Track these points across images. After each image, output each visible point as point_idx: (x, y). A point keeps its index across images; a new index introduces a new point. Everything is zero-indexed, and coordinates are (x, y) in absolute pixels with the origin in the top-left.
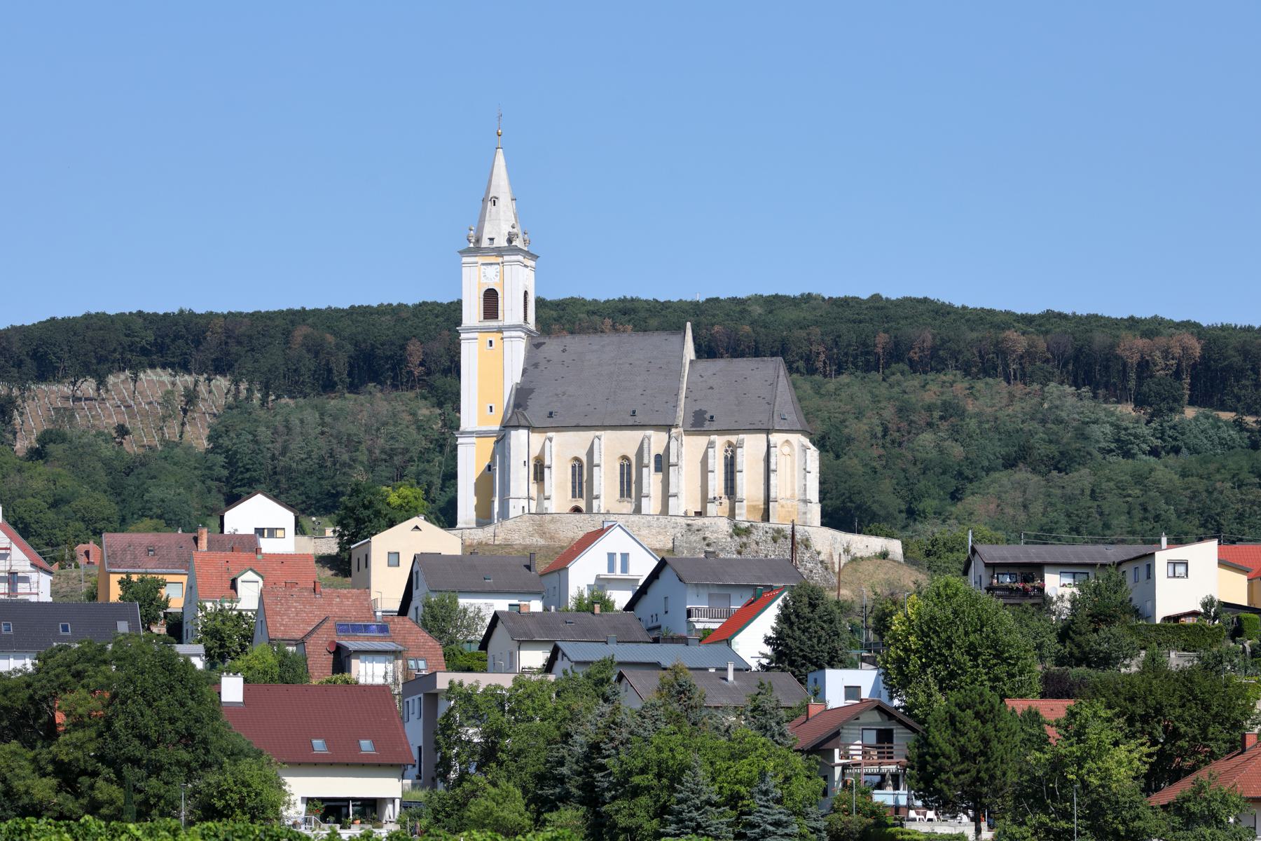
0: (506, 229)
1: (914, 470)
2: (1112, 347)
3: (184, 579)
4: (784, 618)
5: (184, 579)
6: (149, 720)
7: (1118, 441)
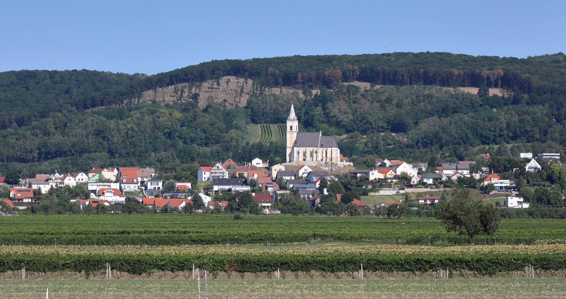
0: (293, 117)
1: (419, 112)
2: (480, 73)
3: (247, 173)
4: (321, 182)
5: (247, 173)
6: (246, 199)
7: (471, 103)
